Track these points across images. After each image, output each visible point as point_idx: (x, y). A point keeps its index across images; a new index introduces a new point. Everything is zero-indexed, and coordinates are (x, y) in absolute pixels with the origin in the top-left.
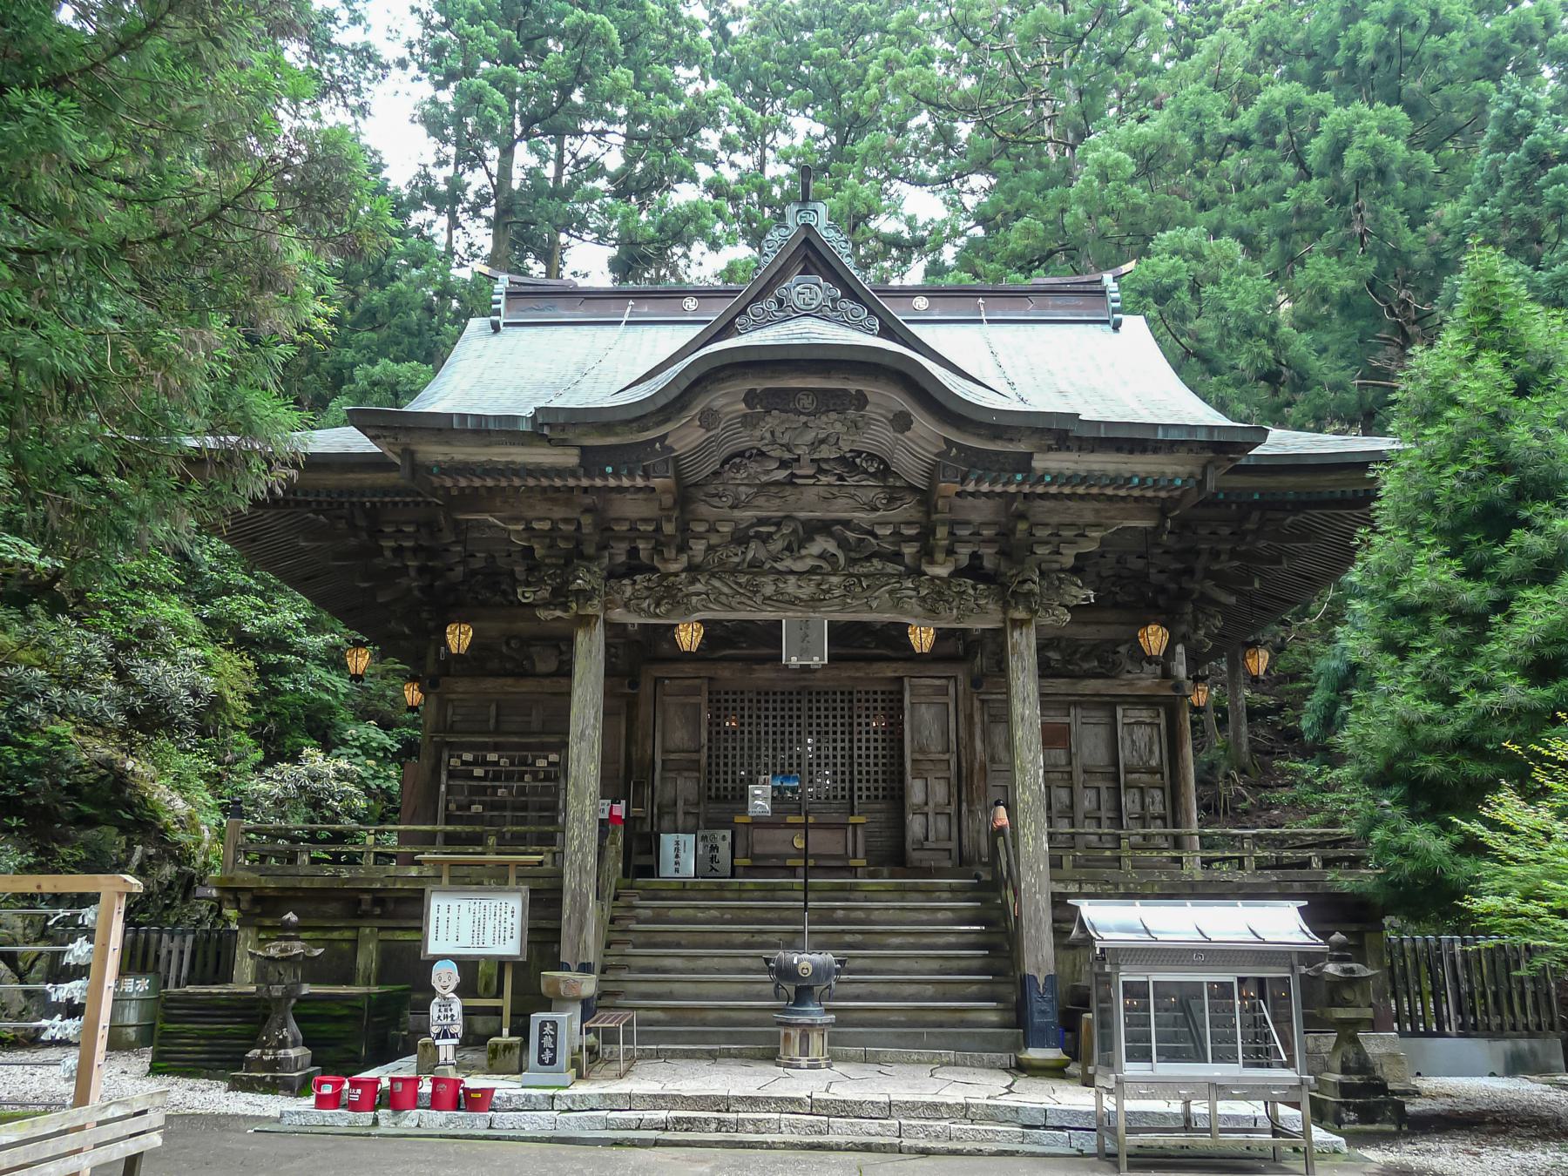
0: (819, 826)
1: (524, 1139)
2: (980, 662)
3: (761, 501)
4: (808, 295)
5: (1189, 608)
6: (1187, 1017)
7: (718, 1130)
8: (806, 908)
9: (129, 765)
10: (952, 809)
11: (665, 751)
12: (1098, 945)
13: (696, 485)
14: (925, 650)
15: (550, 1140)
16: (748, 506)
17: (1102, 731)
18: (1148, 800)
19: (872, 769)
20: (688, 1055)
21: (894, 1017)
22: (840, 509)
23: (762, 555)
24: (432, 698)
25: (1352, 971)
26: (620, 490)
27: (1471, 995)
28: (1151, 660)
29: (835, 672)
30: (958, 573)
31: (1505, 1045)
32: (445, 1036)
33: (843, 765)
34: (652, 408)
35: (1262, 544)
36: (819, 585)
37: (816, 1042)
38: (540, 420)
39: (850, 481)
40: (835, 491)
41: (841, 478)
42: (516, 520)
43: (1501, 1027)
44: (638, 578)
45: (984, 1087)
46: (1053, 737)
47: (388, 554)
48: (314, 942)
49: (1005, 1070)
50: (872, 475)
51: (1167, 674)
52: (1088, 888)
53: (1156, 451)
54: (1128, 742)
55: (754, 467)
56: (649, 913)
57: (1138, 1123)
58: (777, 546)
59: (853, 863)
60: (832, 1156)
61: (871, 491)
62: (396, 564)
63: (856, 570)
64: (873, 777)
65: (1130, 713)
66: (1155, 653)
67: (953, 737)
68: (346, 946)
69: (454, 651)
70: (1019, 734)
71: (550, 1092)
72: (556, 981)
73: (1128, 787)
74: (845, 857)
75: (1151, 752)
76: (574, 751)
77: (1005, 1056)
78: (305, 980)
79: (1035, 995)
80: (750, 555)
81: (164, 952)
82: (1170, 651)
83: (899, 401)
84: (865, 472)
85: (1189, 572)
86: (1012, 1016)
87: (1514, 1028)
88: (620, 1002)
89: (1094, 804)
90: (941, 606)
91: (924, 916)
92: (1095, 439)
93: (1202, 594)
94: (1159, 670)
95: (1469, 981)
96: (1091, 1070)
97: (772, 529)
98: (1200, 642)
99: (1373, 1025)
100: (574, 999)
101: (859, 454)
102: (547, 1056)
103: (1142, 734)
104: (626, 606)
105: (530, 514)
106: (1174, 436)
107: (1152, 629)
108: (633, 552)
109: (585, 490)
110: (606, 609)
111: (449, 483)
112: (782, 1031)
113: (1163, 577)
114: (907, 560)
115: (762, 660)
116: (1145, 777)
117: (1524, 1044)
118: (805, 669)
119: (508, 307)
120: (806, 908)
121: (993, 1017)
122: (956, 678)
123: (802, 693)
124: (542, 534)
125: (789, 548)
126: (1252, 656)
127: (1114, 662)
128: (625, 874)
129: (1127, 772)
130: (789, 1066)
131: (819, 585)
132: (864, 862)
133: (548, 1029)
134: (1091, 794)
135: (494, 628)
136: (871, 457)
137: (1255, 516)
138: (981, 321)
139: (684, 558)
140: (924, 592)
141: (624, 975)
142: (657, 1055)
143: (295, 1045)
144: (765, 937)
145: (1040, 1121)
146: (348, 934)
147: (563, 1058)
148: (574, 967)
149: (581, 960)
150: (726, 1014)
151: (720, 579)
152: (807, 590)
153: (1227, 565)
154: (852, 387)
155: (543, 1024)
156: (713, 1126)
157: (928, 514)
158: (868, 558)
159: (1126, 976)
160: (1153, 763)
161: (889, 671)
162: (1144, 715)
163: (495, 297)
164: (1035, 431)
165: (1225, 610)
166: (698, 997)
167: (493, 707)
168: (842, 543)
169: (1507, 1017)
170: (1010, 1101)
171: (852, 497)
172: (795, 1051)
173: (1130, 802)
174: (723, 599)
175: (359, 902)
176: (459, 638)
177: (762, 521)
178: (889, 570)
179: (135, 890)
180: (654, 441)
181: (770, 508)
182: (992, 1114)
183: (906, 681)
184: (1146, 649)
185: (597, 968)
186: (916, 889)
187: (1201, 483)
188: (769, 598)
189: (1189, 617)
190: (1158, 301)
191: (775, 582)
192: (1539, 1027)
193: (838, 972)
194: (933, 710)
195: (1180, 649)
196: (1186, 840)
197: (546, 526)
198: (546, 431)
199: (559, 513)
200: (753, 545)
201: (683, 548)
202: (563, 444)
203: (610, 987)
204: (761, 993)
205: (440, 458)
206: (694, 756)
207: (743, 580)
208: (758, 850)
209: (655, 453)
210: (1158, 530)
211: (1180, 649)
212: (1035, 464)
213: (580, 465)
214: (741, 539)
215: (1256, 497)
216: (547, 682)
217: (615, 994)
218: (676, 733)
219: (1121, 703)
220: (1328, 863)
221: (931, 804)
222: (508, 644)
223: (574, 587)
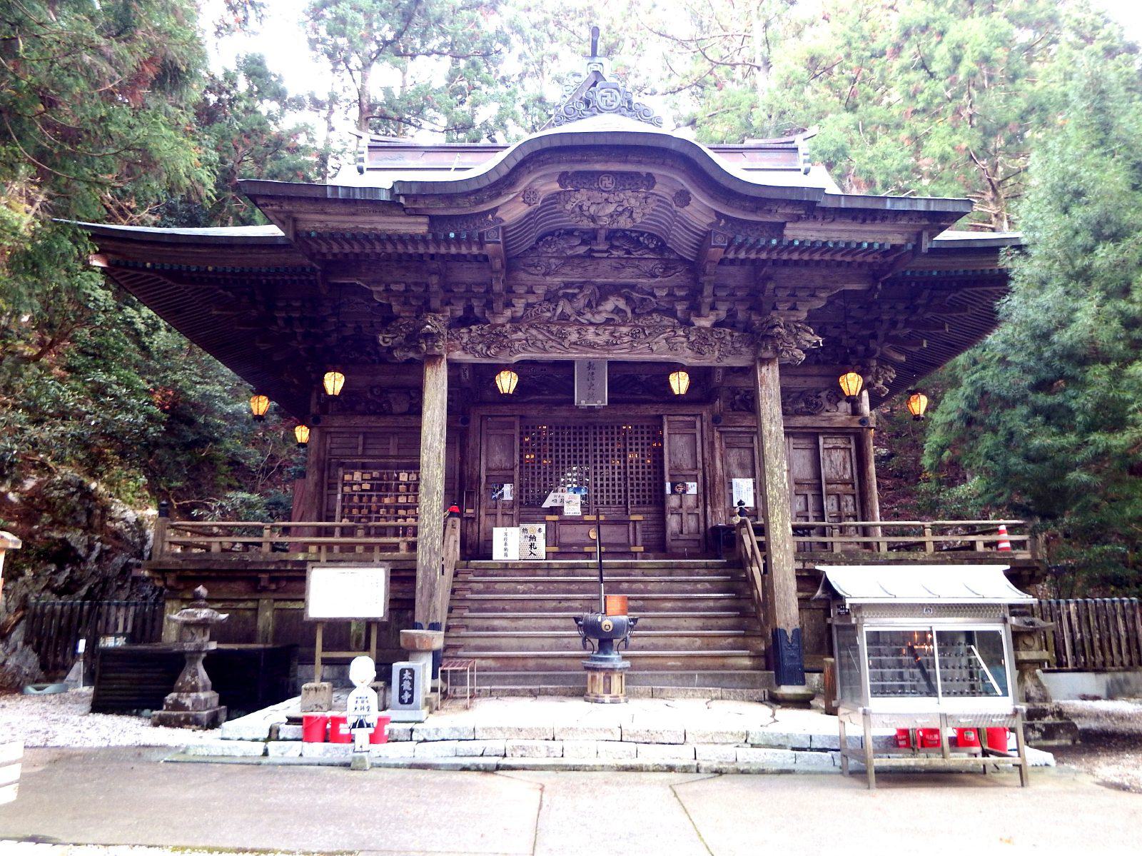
0: (607, 522)
1: (388, 766)
3: (567, 270)
4: (609, 98)
5: (874, 363)
9: (93, 485)
10: (700, 511)
11: (488, 469)
12: (848, 601)
13: (517, 257)
14: (683, 392)
15: (411, 766)
16: (556, 273)
18: (843, 504)
19: (641, 482)
20: (513, 693)
21: (671, 663)
22: (627, 276)
23: (568, 310)
24: (315, 430)
25: (1032, 623)
26: (459, 258)
27: (1082, 640)
29: (613, 412)
30: (717, 324)
31: (1105, 678)
34: (486, 183)
35: (928, 315)
37: (616, 681)
38: (397, 191)
39: (636, 255)
40: (623, 262)
41: (628, 252)
42: (378, 283)
43: (1104, 664)
44: (473, 328)
47: (281, 323)
48: (221, 610)
49: (761, 702)
50: (652, 250)
53: (883, 219)
54: (827, 462)
55: (562, 244)
56: (481, 586)
58: (581, 302)
59: (634, 549)
60: (644, 775)
61: (651, 262)
62: (288, 331)
63: (641, 322)
64: (641, 488)
65: (829, 441)
67: (699, 458)
68: (249, 614)
69: (330, 392)
70: (768, 445)
71: (409, 726)
72: (413, 637)
73: (828, 494)
74: (628, 545)
75: (845, 468)
76: (424, 473)
77: (760, 692)
78: (212, 639)
79: (784, 644)
80: (559, 310)
81: (112, 619)
83: (683, 182)
84: (647, 247)
85: (874, 336)
86: (763, 662)
87: (1113, 665)
88: (460, 653)
89: (803, 507)
90: (705, 349)
91: (688, 587)
92: (836, 209)
93: (882, 354)
95: (1081, 631)
96: (834, 703)
97: (576, 291)
98: (879, 389)
100: (427, 651)
101: (642, 234)
102: (407, 696)
104: (464, 349)
105: (389, 279)
107: (851, 375)
108: (469, 309)
109: (432, 257)
110: (449, 352)
111: (324, 249)
112: (590, 675)
113: (853, 342)
114: (679, 314)
115: (559, 403)
116: (841, 487)
117: (1120, 676)
118: (591, 409)
120: (602, 581)
121: (747, 662)
123: (590, 423)
124: (398, 295)
125: (589, 305)
128: (462, 558)
129: (828, 483)
130: (596, 701)
132: (642, 549)
133: (407, 675)
135: (361, 381)
136: (652, 236)
137: (926, 293)
139: (508, 313)
140: (692, 339)
141: (463, 632)
142: (490, 694)
143: (205, 689)
144: (569, 604)
146: (250, 605)
147: (419, 697)
148: (426, 626)
149: (431, 621)
150: (543, 661)
151: (536, 328)
152: (605, 337)
153: (902, 331)
154: (643, 169)
155: (402, 671)
157: (696, 280)
158: (650, 313)
159: (871, 624)
160: (847, 477)
161: (651, 411)
162: (840, 442)
164: (789, 202)
165: (896, 365)
166: (521, 649)
167: (361, 438)
168: (628, 299)
169: (1108, 657)
171: (637, 267)
172: (599, 690)
173: (830, 505)
174: (539, 344)
175: (259, 580)
176: (334, 383)
177: (567, 285)
178: (665, 323)
179: (11, 546)
181: (575, 276)
183: (665, 419)
185: (443, 628)
186: (680, 567)
188: (575, 343)
192: (1131, 663)
194: (685, 438)
196: (871, 530)
197: (402, 288)
198: (402, 200)
199: (411, 278)
200: (561, 303)
201: (509, 304)
202: (417, 213)
203: (451, 642)
204: (574, 644)
205: (317, 225)
206: (510, 473)
207: (554, 329)
208: (564, 540)
209: (490, 223)
210: (872, 289)
212: (786, 232)
213: (429, 232)
214: (552, 297)
215: (935, 273)
216: (401, 419)
217: (456, 647)
218: (494, 456)
219: (823, 434)
222: (372, 392)
223: (424, 330)
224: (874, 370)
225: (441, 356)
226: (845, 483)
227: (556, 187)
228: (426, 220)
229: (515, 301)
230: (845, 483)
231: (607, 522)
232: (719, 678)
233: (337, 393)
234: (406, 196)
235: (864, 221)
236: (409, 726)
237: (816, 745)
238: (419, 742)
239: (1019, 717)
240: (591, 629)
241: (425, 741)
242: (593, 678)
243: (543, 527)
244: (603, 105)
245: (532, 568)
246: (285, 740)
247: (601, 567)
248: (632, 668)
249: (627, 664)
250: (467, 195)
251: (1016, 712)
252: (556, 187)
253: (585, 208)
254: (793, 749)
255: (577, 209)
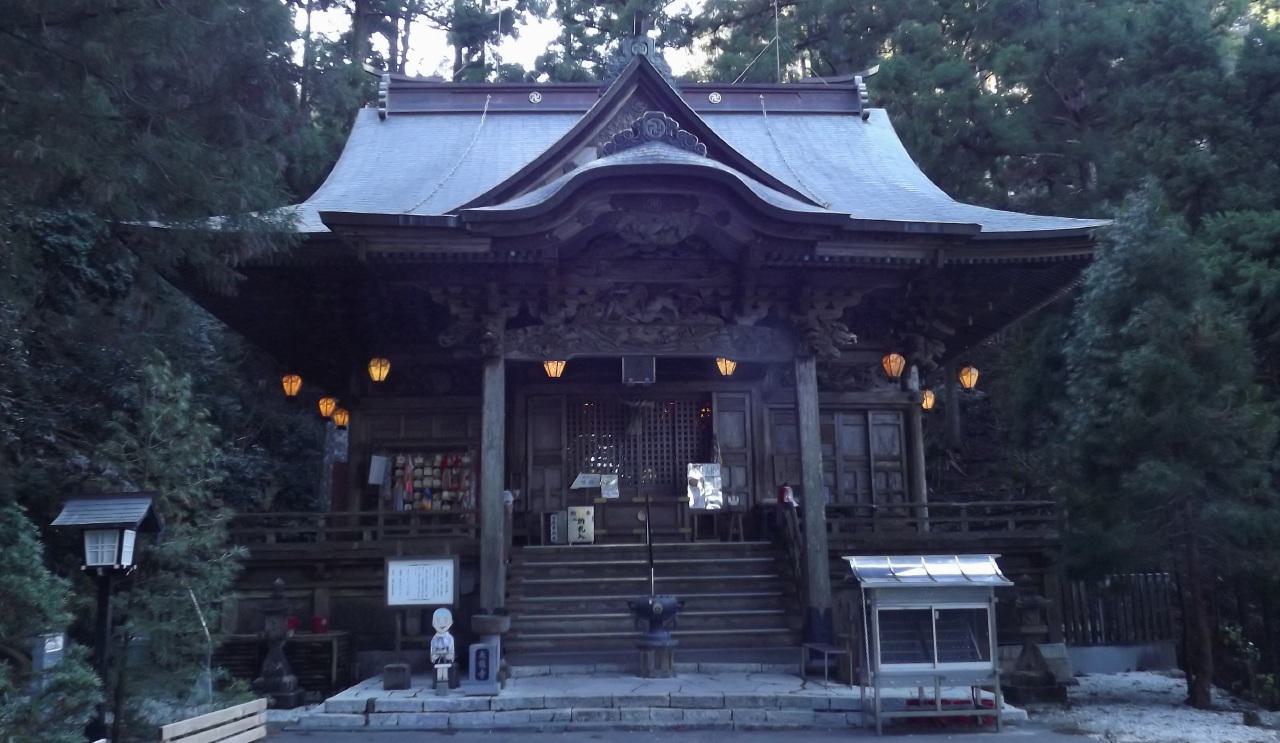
0: (655, 504)
2: (769, 380)
6: (914, 630)
7: (607, 720)
8: (652, 564)
10: (749, 490)
17: (857, 431)
18: (891, 481)
23: (620, 311)
28: (891, 380)
32: (442, 662)
33: (668, 458)
36: (661, 332)
38: (464, 219)
44: (529, 329)
45: (787, 687)
46: (827, 435)
51: (905, 388)
52: (850, 547)
57: (889, 703)
59: (682, 530)
66: (894, 374)
71: (488, 698)
75: (893, 445)
82: (906, 372)
94: (899, 385)
99: (1047, 639)
100: (497, 634)
102: (482, 673)
103: (887, 432)
106: (917, 229)
107: (893, 356)
108: (523, 311)
116: (889, 464)
119: (391, 100)
120: (652, 564)
121: (787, 640)
122: (750, 392)
125: (638, 305)
126: (966, 374)
127: (866, 380)
131: (661, 332)
133: (482, 654)
134: (850, 477)
138: (761, 113)
140: (736, 337)
145: (826, 706)
146: (305, 593)
154: (689, 192)
156: (604, 717)
162: (889, 418)
163: (381, 92)
168: (675, 297)
170: (805, 694)
176: (379, 372)
177: (617, 285)
180: (547, 232)
182: (792, 702)
184: (889, 372)
187: (934, 262)
188: (625, 343)
189: (921, 346)
190: (893, 93)
191: (629, 331)
192: (1095, 634)
193: (681, 609)
195: (914, 369)
198: (468, 227)
203: (518, 625)
207: (607, 328)
211: (914, 369)
214: (603, 298)
220: (1018, 524)
221: (734, 486)
223: (485, 337)
224: (921, 346)
225: (498, 357)
226: (893, 459)
227: (607, 208)
228: (488, 241)
229: (567, 302)
230: (893, 459)
231: (655, 504)
232: (758, 651)
233: (382, 379)
234: (472, 223)
235: (886, 240)
236: (488, 698)
237: (835, 706)
238: (497, 711)
239: (997, 678)
240: (642, 611)
241: (502, 710)
242: (645, 656)
243: (591, 509)
244: (650, 134)
245: (720, 357)
246: (380, 712)
247: (650, 552)
248: (679, 646)
249: (675, 642)
250: (528, 220)
251: (995, 672)
252: (607, 208)
253: (635, 227)
254: (816, 710)
255: (628, 229)
